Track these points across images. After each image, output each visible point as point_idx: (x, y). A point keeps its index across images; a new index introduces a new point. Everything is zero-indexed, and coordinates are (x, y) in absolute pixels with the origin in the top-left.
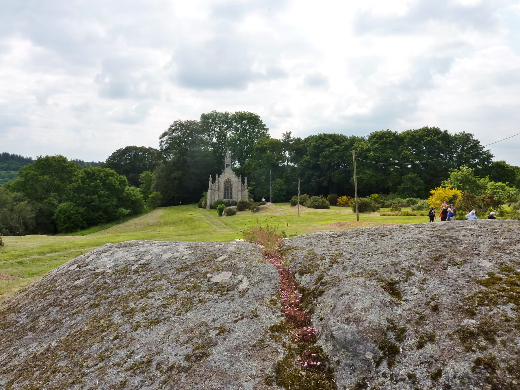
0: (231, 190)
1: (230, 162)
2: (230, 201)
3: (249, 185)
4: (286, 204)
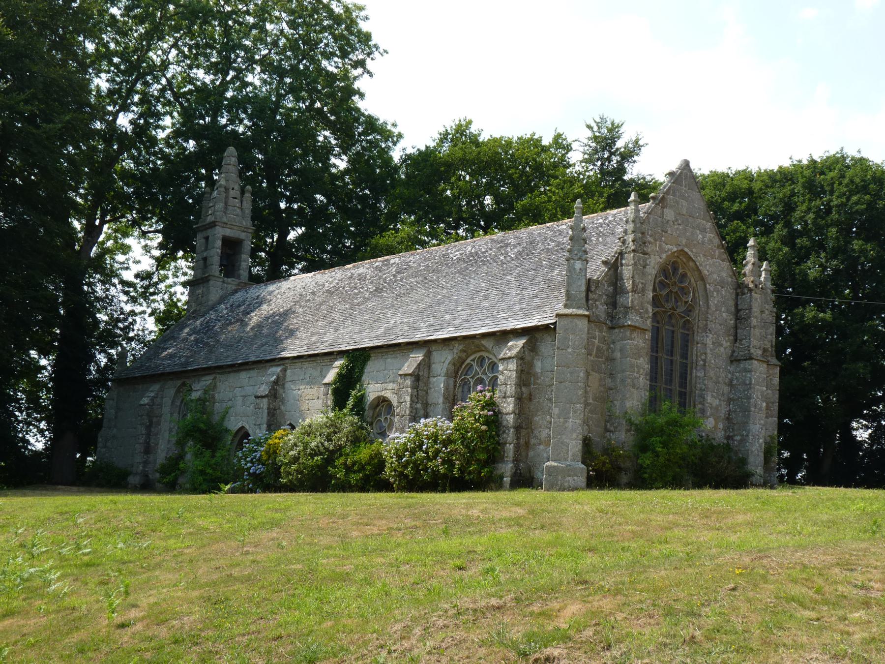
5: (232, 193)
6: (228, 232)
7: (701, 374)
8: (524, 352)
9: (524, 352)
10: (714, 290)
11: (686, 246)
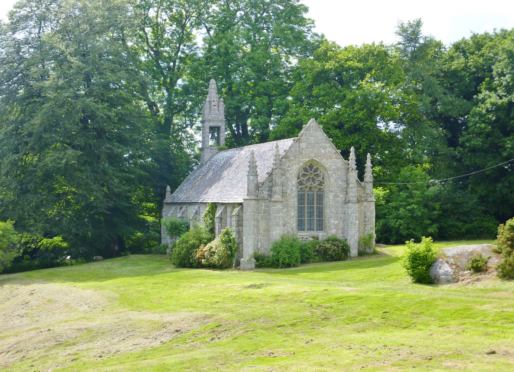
0: (320, 198)
1: (221, 121)
2: (317, 238)
3: (377, 182)
4: (450, 243)
5: (213, 103)
6: (212, 124)
7: (328, 211)
8: (239, 213)
9: (239, 213)
10: (333, 173)
11: (315, 157)
